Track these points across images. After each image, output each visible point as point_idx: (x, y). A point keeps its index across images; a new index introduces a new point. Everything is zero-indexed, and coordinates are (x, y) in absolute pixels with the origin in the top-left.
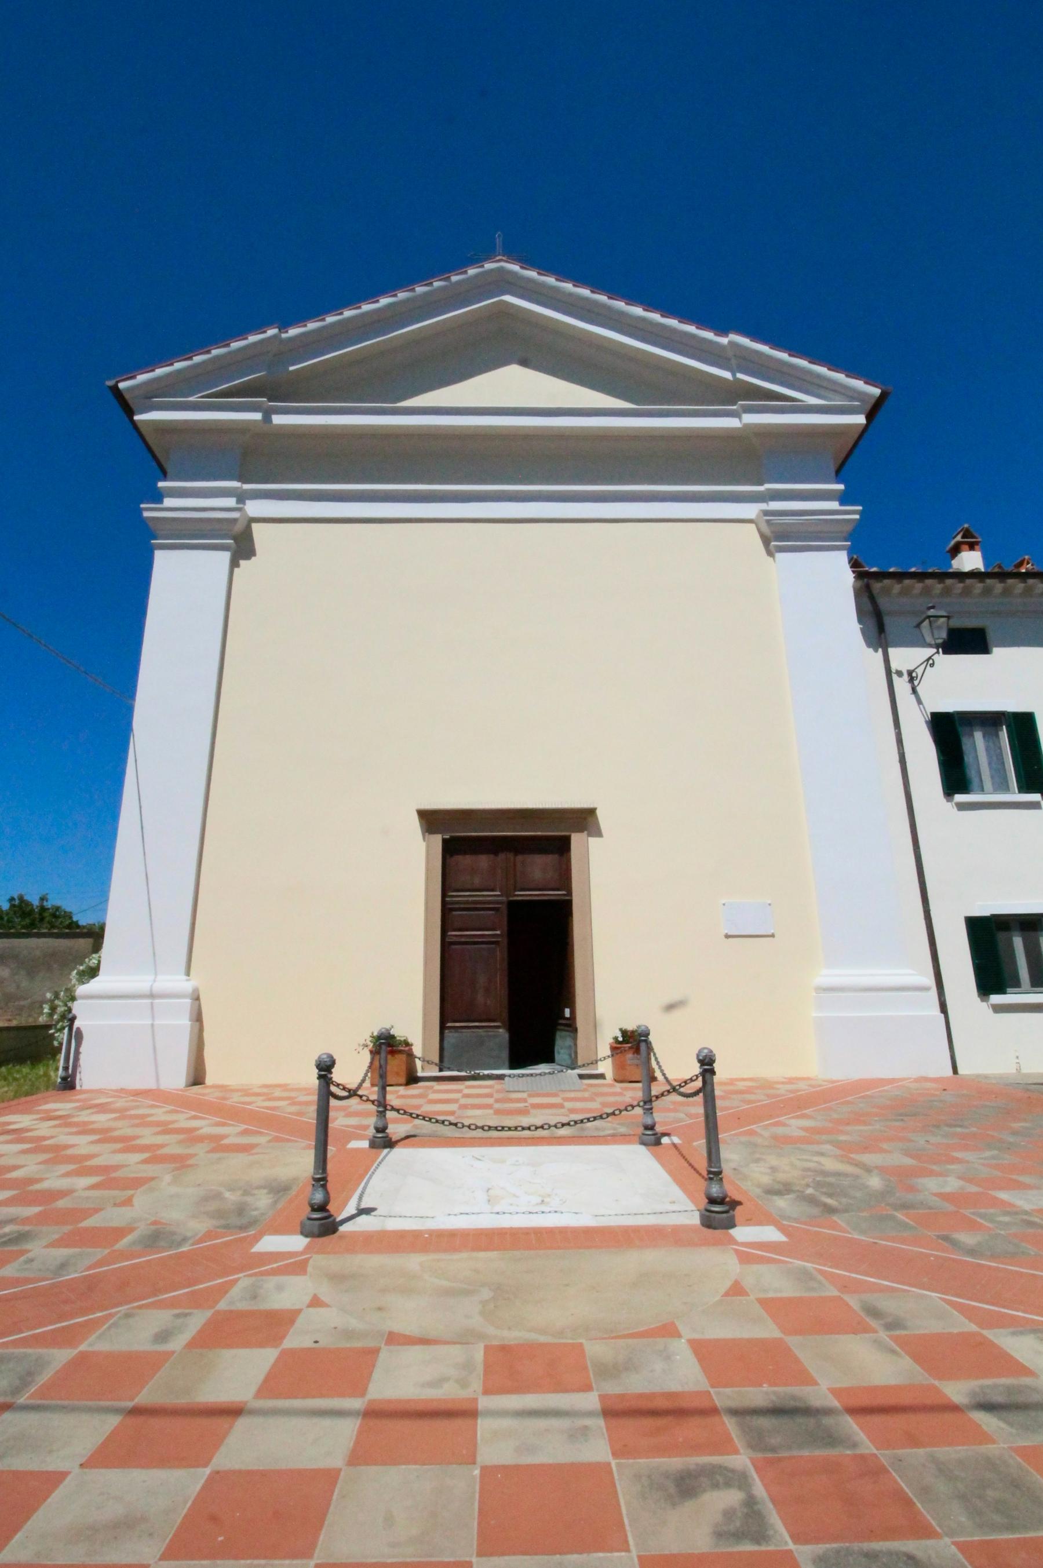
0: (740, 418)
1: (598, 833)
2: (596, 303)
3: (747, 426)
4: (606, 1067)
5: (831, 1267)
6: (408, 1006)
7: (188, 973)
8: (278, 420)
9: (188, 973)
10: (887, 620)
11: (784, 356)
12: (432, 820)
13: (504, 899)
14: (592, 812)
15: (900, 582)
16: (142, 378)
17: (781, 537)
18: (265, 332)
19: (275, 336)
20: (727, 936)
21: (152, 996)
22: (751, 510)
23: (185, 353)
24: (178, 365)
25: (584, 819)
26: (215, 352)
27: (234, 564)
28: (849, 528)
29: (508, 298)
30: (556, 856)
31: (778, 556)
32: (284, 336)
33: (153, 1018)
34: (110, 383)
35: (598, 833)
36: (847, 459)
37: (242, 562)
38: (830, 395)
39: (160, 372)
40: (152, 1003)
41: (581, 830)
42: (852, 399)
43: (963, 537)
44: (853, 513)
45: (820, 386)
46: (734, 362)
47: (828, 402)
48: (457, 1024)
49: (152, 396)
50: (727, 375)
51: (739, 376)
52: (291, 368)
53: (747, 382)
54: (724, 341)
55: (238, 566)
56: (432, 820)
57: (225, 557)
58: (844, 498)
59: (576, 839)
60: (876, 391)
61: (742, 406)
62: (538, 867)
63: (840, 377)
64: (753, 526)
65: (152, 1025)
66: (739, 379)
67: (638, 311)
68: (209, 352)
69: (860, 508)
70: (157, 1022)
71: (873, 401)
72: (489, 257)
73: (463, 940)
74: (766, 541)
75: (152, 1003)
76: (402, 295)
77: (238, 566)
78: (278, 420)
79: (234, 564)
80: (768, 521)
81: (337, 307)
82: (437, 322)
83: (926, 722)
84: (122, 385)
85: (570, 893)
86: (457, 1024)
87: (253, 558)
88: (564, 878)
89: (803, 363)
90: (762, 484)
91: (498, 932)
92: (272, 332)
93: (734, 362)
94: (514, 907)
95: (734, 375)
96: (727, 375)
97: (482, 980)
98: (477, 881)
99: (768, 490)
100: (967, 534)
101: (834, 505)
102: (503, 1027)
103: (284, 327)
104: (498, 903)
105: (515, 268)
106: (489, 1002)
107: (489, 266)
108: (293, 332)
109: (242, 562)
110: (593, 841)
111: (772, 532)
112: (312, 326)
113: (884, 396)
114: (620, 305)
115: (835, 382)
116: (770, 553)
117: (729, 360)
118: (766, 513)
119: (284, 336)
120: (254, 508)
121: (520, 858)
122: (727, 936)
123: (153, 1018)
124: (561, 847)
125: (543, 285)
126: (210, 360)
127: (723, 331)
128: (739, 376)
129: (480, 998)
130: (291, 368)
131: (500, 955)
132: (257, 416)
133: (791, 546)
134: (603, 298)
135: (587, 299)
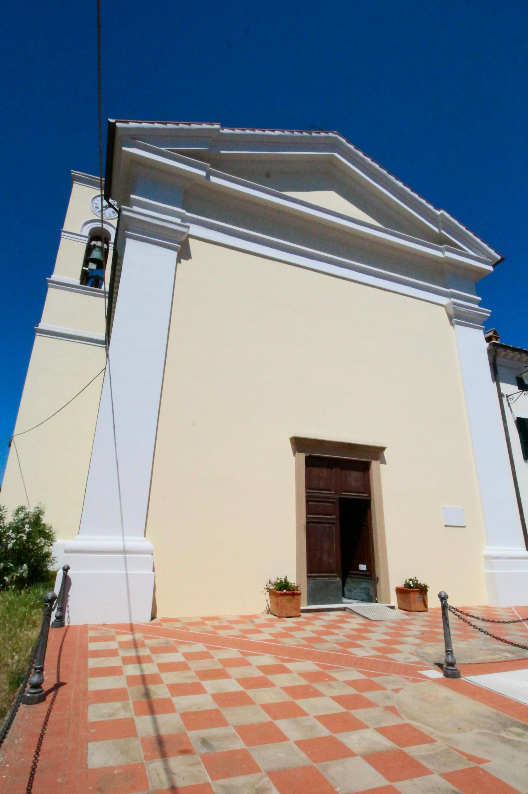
0: (443, 254)
1: (384, 462)
2: (381, 173)
3: (447, 257)
4: (394, 601)
5: (206, 635)
6: (290, 565)
7: (145, 536)
8: (214, 179)
9: (145, 536)
10: (499, 369)
11: (463, 228)
12: (299, 444)
13: (337, 496)
14: (383, 449)
15: (513, 352)
16: (132, 125)
17: (457, 317)
18: (213, 125)
19: (217, 130)
20: (446, 526)
21: (125, 552)
22: (445, 301)
23: (164, 119)
24: (157, 125)
25: (377, 452)
26: (181, 126)
27: (178, 261)
28: (485, 319)
29: (336, 155)
30: (362, 473)
31: (457, 326)
32: (221, 131)
33: (126, 569)
34: (112, 121)
35: (384, 462)
36: (483, 285)
37: (183, 261)
38: (478, 252)
39: (145, 125)
40: (125, 558)
41: (377, 459)
42: (489, 258)
43: (494, 334)
44: (487, 313)
45: (477, 248)
46: (440, 224)
47: (478, 257)
48: (314, 575)
49: (135, 138)
50: (436, 230)
51: (443, 232)
52: (222, 152)
53: (446, 236)
54: (439, 213)
55: (180, 262)
56: (299, 444)
57: (175, 254)
58: (480, 304)
59: (374, 464)
60: (499, 257)
61: (446, 247)
62: (353, 477)
63: (485, 246)
64: (443, 308)
65: (127, 574)
66: (442, 234)
67: (400, 184)
68: (178, 124)
69: (490, 311)
70: (129, 572)
71: (497, 261)
72: (331, 130)
73: (316, 520)
74: (450, 318)
75: (125, 558)
76: (287, 133)
77: (180, 262)
78: (214, 179)
79: (178, 261)
80: (454, 308)
81: (253, 127)
82: (325, 155)
83: (515, 422)
84: (118, 125)
85: (370, 496)
86: (314, 575)
87: (190, 260)
88: (366, 486)
89: (471, 234)
90: (448, 288)
91: (334, 517)
92: (216, 126)
93: (440, 224)
94: (343, 502)
95: (439, 230)
96: (436, 230)
97: (326, 546)
98: (322, 484)
99: (451, 292)
100: (495, 333)
101: (476, 306)
102: (340, 577)
103: (223, 126)
104: (334, 499)
105: (344, 141)
106: (330, 561)
107: (331, 134)
108: (226, 131)
109: (183, 261)
110: (382, 466)
111: (454, 314)
112: (237, 131)
113: (502, 259)
114: (392, 178)
115: (481, 246)
116: (452, 324)
117: (438, 222)
118: (454, 304)
119: (221, 131)
120: (195, 230)
121: (344, 471)
122: (446, 526)
123: (126, 569)
124: (365, 467)
125: (356, 154)
126: (176, 129)
127: (438, 208)
128: (443, 232)
129: (325, 557)
130: (222, 152)
131: (335, 530)
132: (203, 173)
133: (466, 324)
134: (384, 172)
135: (376, 170)
